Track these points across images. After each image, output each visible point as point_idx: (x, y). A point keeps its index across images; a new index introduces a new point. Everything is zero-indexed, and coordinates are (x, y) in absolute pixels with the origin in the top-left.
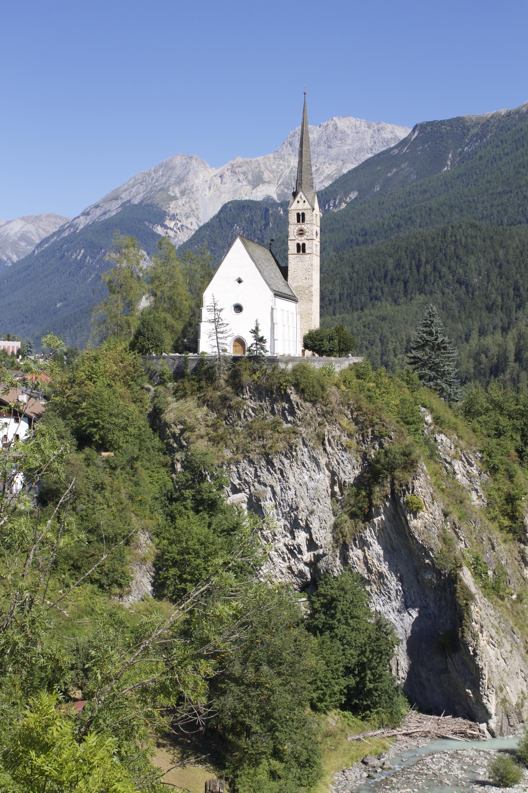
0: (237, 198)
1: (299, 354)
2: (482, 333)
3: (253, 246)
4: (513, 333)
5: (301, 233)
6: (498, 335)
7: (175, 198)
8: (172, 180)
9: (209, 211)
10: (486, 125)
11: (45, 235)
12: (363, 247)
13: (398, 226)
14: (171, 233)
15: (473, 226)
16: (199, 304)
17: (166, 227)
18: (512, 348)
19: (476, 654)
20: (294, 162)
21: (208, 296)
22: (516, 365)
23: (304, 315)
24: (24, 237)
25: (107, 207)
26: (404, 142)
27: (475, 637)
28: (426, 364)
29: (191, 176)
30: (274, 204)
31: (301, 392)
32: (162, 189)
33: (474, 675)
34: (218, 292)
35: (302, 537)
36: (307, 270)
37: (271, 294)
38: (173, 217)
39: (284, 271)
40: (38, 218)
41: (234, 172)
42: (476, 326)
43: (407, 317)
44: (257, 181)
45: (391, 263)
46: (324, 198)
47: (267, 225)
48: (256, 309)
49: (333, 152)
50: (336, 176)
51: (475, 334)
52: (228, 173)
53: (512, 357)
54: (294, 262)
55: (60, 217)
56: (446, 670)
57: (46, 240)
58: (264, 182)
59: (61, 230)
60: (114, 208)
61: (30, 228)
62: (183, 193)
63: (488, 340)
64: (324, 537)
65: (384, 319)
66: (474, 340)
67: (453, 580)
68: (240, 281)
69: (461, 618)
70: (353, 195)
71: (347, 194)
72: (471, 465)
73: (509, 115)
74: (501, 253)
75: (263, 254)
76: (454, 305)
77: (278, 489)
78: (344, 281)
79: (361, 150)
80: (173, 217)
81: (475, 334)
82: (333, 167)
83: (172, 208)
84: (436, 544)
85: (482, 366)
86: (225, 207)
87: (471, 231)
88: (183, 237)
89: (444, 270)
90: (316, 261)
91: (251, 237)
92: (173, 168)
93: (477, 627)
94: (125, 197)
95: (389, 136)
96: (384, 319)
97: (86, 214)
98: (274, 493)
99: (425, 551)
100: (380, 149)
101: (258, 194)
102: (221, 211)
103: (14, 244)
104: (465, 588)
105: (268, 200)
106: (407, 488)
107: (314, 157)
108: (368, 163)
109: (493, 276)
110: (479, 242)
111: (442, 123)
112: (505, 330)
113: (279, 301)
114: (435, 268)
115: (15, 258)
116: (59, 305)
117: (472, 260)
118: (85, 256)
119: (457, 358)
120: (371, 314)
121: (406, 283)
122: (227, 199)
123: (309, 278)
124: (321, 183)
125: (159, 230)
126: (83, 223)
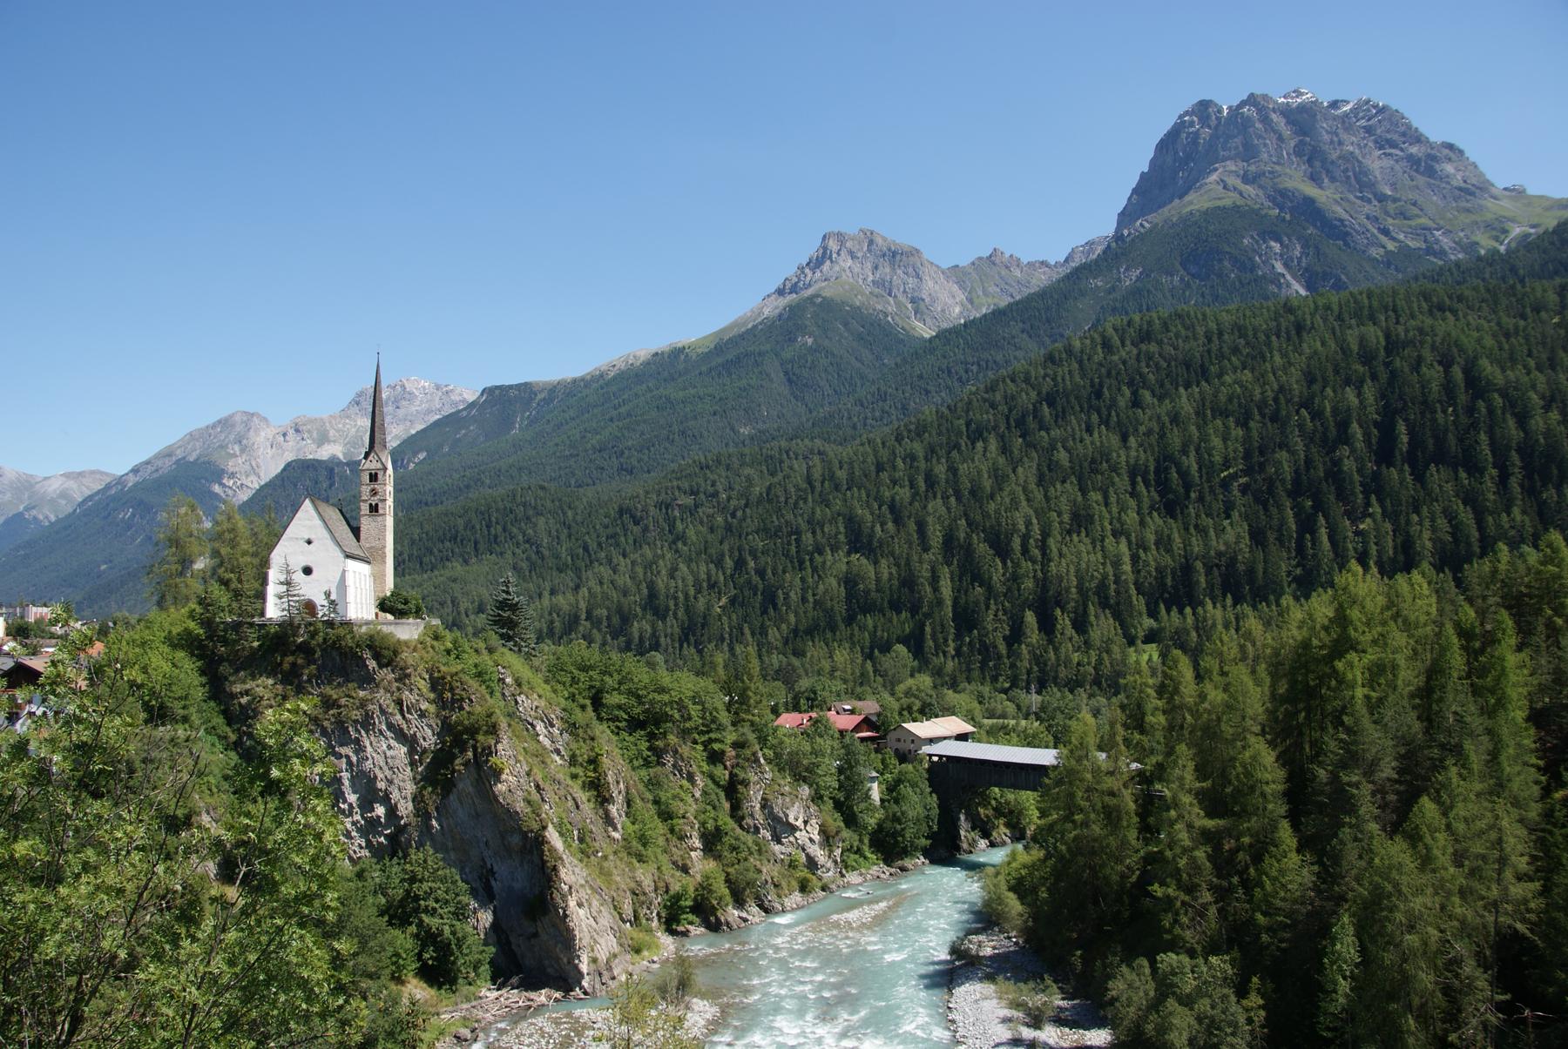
0: (301, 457)
1: (372, 617)
2: (553, 592)
3: (323, 507)
4: (584, 591)
5: (374, 493)
6: (570, 596)
7: (235, 456)
8: (232, 437)
9: (271, 467)
10: (553, 390)
11: (88, 493)
12: (433, 509)
13: (468, 487)
14: (230, 492)
15: (542, 488)
16: (265, 564)
17: (224, 486)
18: (583, 605)
19: (566, 916)
20: (366, 423)
21: (277, 557)
22: (588, 624)
23: (378, 578)
24: (64, 494)
25: (160, 463)
26: (472, 405)
27: (564, 897)
28: (506, 622)
29: (252, 433)
30: (340, 463)
31: (377, 656)
32: (221, 447)
33: (566, 939)
34: (286, 554)
35: (380, 811)
36: (384, 531)
37: (341, 556)
38: (232, 475)
39: (356, 532)
40: (81, 474)
41: (297, 431)
42: (547, 585)
43: (482, 579)
44: (323, 439)
45: (460, 522)
46: (397, 456)
47: (331, 485)
48: (331, 573)
49: (401, 412)
50: (405, 437)
51: (546, 594)
52: (292, 431)
53: (583, 616)
54: (366, 524)
55: (107, 474)
56: (536, 935)
57: (90, 498)
58: (329, 441)
59: (108, 487)
60: (167, 464)
61: (72, 484)
62: (243, 451)
63: (560, 600)
64: (406, 808)
65: (454, 581)
66: (546, 601)
67: (539, 841)
68: (309, 542)
69: (550, 880)
70: (422, 456)
71: (415, 454)
72: (552, 726)
73: (574, 381)
74: (570, 513)
75: (333, 515)
76: (524, 565)
77: (354, 759)
78: (413, 542)
79: (429, 411)
80: (232, 475)
81: (546, 594)
82: (401, 427)
83: (231, 466)
84: (520, 806)
85: (1206, 705)
86: (288, 465)
87: (541, 493)
88: (244, 496)
89: (515, 530)
90: (390, 521)
91: (319, 497)
92: (233, 426)
93: (566, 888)
94: (179, 454)
95: (458, 398)
96: (454, 581)
97: (135, 471)
98: (350, 763)
99: (513, 815)
100: (448, 410)
101: (324, 453)
102: (284, 470)
103: (52, 501)
104: (553, 850)
105: (333, 458)
106: (489, 751)
107: (388, 419)
108: (436, 424)
109: (563, 537)
110: (548, 504)
111: (511, 387)
112: (577, 588)
113: (349, 561)
114: (504, 530)
115: (53, 519)
116: (103, 567)
117: (541, 521)
118: (133, 515)
119: (532, 616)
120: (440, 576)
121: (476, 543)
122: (290, 457)
123: (382, 538)
124: (392, 443)
125: (217, 488)
126: (132, 481)
